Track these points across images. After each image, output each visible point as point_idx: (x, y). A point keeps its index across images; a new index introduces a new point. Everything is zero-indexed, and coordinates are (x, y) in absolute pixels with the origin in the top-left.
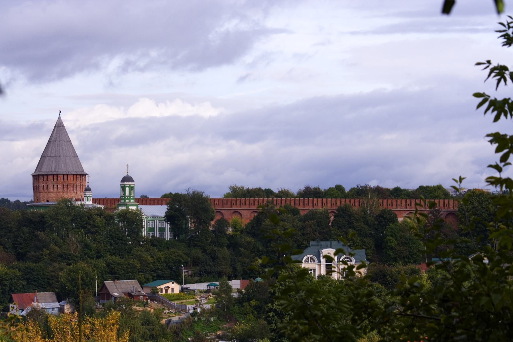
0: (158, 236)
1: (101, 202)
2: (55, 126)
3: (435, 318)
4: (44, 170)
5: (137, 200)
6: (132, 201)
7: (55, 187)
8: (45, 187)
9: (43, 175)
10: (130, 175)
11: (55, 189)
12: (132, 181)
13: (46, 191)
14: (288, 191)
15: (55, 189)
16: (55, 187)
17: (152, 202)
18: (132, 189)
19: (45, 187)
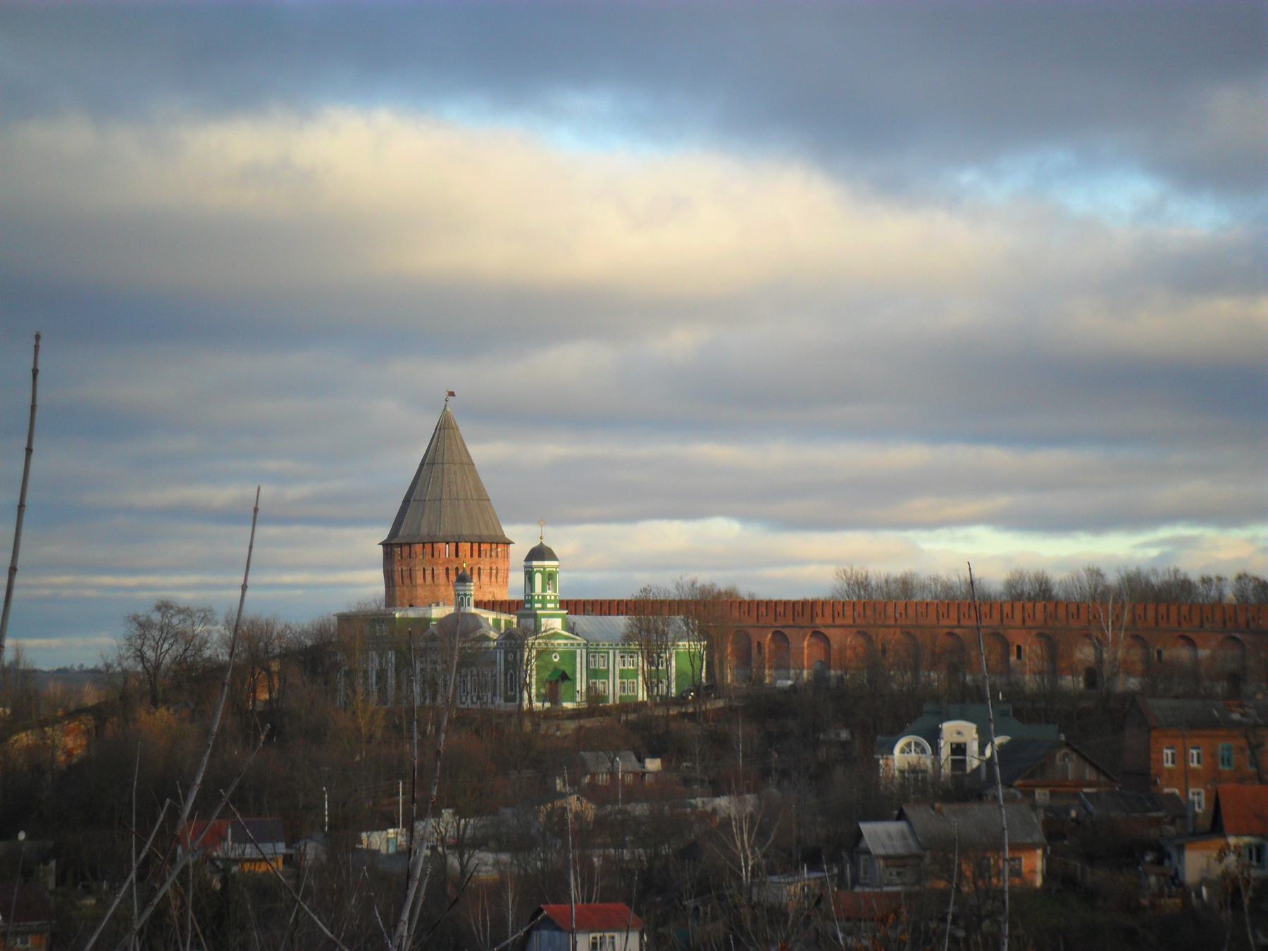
0: (947, 769)
1: (622, 608)
2: (422, 465)
3: (955, 880)
4: (395, 541)
5: (564, 604)
6: (549, 606)
7: (428, 573)
8: (406, 574)
9: (401, 545)
10: (547, 544)
11: (429, 578)
12: (552, 556)
13: (407, 581)
14: (1138, 568)
15: (429, 578)
16: (428, 573)
17: (622, 608)
18: (550, 577)
19: (406, 574)
